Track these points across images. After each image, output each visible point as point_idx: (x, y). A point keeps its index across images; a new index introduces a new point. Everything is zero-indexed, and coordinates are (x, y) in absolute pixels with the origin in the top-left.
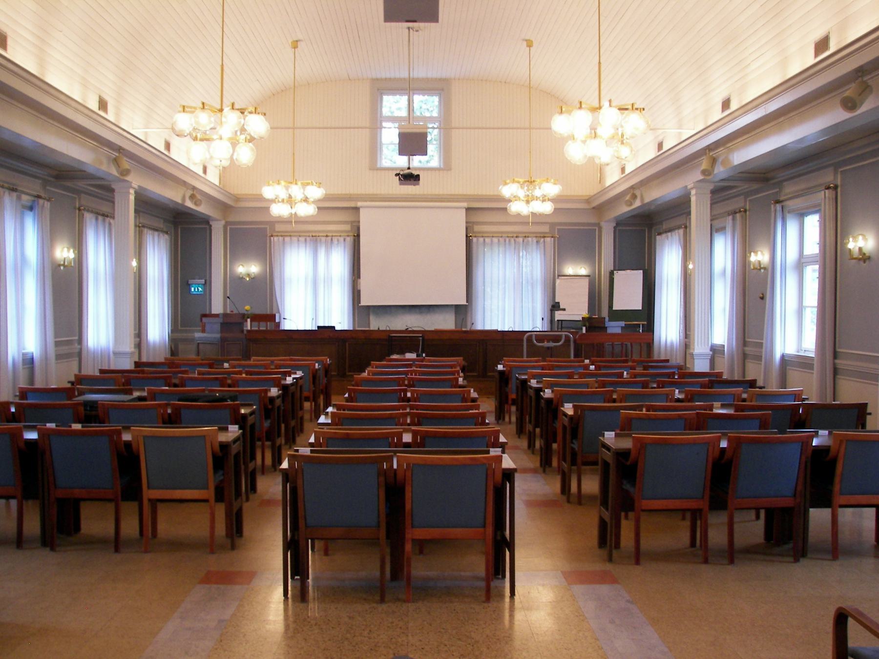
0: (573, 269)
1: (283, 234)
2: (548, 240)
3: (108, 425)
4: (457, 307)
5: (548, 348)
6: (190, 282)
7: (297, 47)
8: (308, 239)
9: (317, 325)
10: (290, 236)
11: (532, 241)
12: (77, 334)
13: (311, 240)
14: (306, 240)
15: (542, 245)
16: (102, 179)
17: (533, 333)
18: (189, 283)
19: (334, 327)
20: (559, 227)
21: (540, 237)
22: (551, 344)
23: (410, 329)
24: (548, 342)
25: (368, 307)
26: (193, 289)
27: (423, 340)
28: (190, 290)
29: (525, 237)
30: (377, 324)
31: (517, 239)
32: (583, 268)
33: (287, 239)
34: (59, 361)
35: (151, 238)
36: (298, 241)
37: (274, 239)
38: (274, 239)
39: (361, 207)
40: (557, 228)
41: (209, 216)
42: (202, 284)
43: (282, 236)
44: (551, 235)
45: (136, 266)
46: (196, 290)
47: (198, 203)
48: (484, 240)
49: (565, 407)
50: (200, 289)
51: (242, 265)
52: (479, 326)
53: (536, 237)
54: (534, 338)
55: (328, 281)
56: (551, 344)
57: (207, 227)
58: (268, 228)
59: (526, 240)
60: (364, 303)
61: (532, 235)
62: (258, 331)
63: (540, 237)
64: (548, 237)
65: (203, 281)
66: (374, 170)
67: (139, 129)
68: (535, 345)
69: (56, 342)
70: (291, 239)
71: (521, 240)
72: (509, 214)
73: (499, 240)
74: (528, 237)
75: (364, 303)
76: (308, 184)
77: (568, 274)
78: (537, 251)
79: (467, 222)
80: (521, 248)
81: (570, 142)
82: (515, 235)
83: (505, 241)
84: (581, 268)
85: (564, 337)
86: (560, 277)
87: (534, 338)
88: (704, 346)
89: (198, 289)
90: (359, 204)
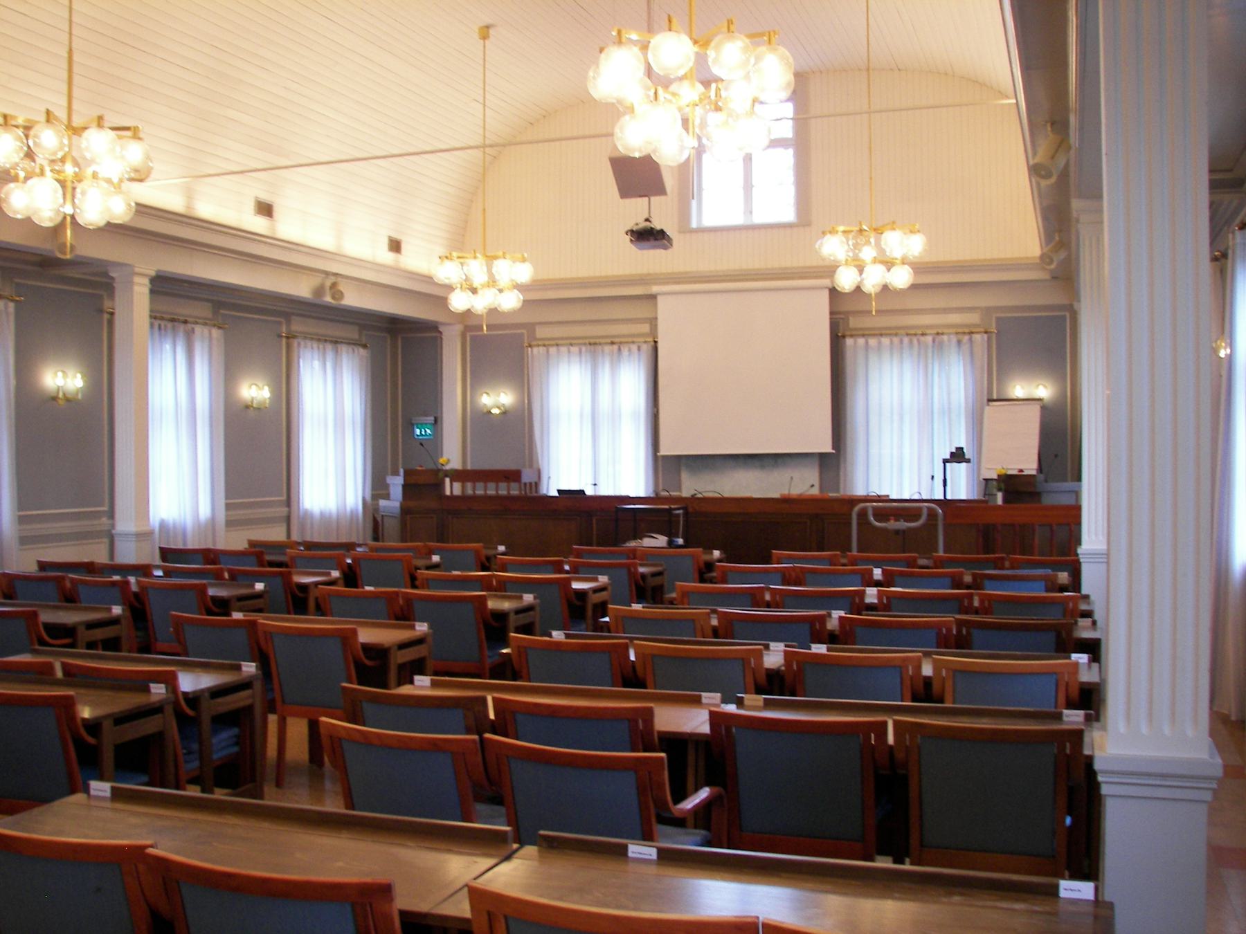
0: (1023, 388)
1: (547, 343)
2: (977, 337)
3: (687, 606)
4: (822, 456)
5: (897, 532)
6: (415, 420)
7: (489, 37)
8: (584, 349)
9: (982, 477)
10: (557, 345)
11: (949, 341)
12: (107, 501)
13: (586, 351)
14: (580, 352)
15: (966, 347)
16: (88, 263)
17: (868, 504)
18: (413, 422)
19: (582, 492)
20: (998, 315)
21: (964, 333)
22: (902, 525)
23: (700, 496)
24: (896, 520)
25: (679, 458)
26: (418, 432)
27: (686, 514)
28: (413, 431)
29: (938, 334)
30: (691, 486)
31: (922, 338)
32: (1041, 387)
33: (553, 350)
34: (24, 547)
35: (895, 370)
36: (569, 352)
37: (532, 351)
38: (532, 351)
39: (659, 294)
40: (1068, 315)
41: (437, 322)
42: (430, 424)
43: (544, 345)
44: (982, 330)
45: (269, 398)
46: (423, 433)
47: (337, 296)
48: (867, 343)
49: (416, 683)
50: (428, 431)
51: (487, 394)
52: (860, 491)
53: (957, 333)
54: (870, 513)
55: (615, 416)
56: (902, 525)
57: (438, 335)
58: (526, 335)
59: (938, 338)
60: (664, 451)
61: (951, 331)
62: (474, 498)
63: (964, 333)
64: (977, 333)
65: (431, 419)
66: (684, 232)
67: (159, 180)
68: (869, 524)
69: (20, 517)
70: (558, 350)
71: (929, 339)
72: (846, 293)
73: (892, 342)
74: (942, 334)
75: (664, 451)
76: (496, 258)
77: (1015, 398)
78: (892, 360)
79: (832, 313)
80: (930, 355)
81: (627, 117)
82: (919, 332)
83: (901, 342)
84: (1038, 385)
85: (925, 512)
86: (991, 403)
87: (870, 513)
88: (1096, 535)
89: (425, 431)
90: (655, 289)
